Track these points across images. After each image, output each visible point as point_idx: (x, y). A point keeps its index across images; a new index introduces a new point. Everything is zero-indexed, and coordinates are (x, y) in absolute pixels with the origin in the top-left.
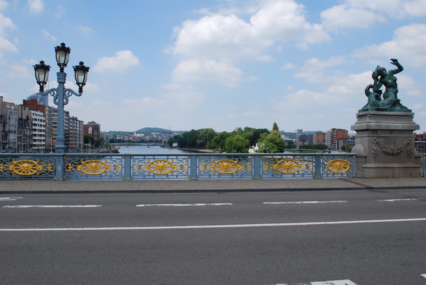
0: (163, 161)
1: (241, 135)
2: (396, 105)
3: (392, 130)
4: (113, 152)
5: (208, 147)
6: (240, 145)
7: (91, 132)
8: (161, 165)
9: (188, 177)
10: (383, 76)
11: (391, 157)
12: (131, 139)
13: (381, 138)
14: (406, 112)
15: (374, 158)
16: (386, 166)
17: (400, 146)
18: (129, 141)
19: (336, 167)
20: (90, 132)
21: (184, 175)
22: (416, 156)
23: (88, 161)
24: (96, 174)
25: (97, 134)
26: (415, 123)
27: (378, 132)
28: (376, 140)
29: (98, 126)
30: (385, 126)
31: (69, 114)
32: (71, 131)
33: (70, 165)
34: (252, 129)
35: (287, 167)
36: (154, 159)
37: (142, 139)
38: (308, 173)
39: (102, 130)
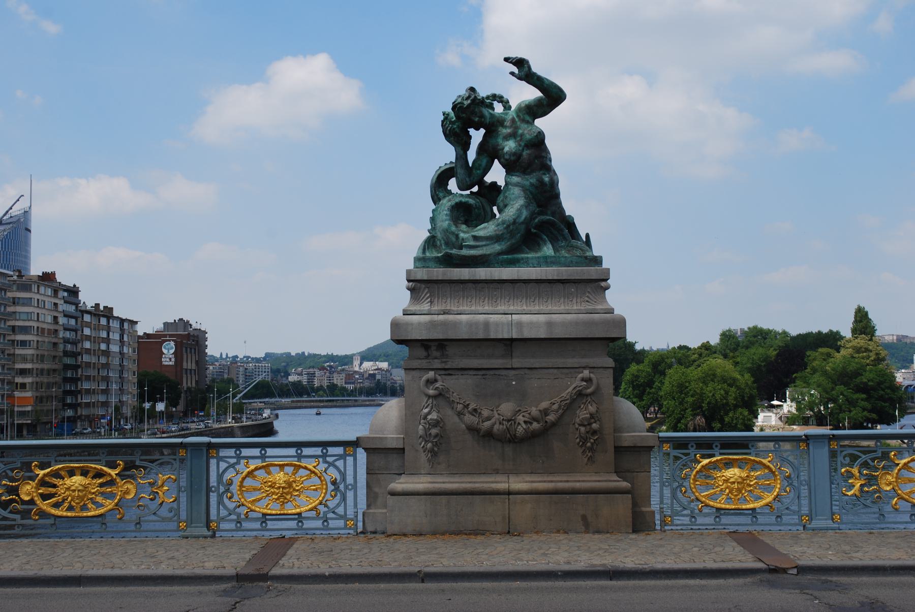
0: (291, 465)
1: (734, 357)
3: (508, 343)
4: (247, 431)
6: (718, 397)
7: (173, 360)
8: (76, 485)
9: (346, 525)
10: (492, 127)
11: (509, 450)
12: (339, 380)
13: (460, 373)
14: (578, 264)
16: (477, 485)
17: (544, 405)
18: (333, 389)
19: (273, 493)
20: (168, 360)
21: (164, 520)
22: (626, 444)
23: (57, 467)
24: (744, 507)
25: (194, 365)
26: (611, 311)
27: (451, 350)
28: (436, 381)
29: (198, 336)
30: (470, 324)
31: (77, 297)
32: (86, 358)
33: (855, 471)
34: (776, 333)
35: (734, 483)
36: (263, 457)
37: (379, 380)
38: (159, 517)
39: (214, 348)
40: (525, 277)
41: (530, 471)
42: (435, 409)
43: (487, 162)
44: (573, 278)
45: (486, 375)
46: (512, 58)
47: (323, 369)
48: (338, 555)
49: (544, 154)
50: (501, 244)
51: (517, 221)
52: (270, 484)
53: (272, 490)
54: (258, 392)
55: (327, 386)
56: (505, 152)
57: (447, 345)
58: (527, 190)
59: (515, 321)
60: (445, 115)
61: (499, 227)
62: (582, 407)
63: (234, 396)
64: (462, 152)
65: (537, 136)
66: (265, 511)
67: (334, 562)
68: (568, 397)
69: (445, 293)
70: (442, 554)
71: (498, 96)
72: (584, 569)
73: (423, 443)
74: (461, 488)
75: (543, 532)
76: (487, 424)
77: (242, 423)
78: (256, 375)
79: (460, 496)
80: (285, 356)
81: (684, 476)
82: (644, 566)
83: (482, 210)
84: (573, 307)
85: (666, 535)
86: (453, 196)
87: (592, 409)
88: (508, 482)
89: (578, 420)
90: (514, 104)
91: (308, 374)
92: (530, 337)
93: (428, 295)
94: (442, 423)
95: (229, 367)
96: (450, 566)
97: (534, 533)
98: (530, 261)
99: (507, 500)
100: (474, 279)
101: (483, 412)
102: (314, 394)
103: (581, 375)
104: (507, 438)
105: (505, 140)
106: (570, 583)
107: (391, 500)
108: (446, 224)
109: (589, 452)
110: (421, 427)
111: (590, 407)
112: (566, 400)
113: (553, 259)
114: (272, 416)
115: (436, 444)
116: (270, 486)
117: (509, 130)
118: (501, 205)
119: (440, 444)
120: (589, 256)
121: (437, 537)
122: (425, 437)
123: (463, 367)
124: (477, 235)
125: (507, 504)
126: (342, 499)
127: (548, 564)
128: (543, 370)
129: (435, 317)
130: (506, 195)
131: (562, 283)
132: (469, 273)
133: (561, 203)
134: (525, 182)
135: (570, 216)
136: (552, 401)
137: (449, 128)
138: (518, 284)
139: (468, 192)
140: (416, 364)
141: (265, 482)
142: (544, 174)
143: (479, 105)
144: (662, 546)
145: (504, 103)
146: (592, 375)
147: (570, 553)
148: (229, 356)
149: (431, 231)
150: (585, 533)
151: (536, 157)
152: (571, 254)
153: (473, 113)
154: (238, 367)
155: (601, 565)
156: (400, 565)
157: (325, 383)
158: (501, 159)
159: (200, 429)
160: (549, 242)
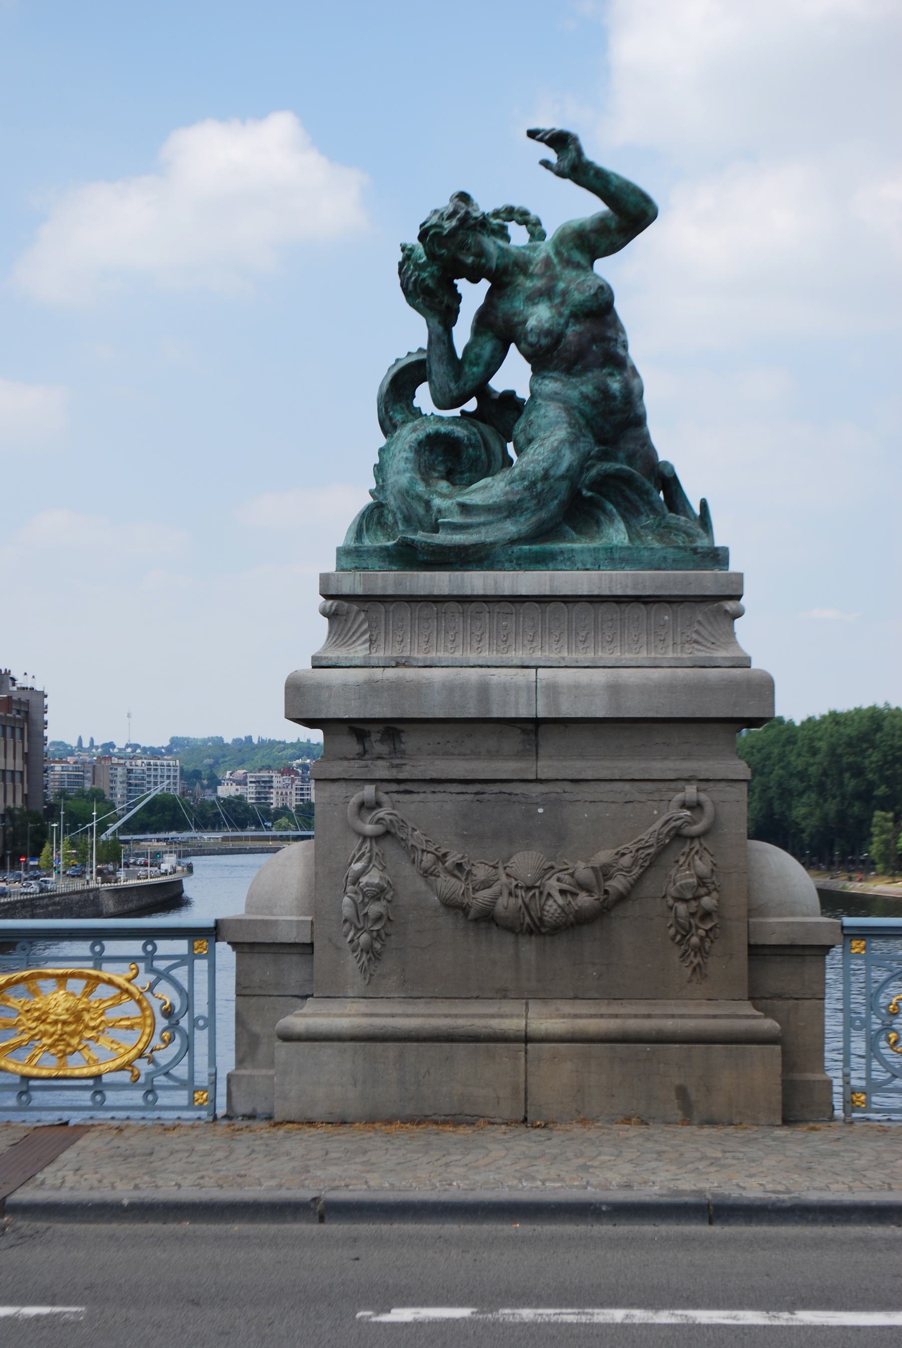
0: (80, 976)
2: (604, 511)
3: (530, 727)
5: (884, 857)
9: (192, 1100)
11: (529, 948)
14: (677, 565)
15: (364, 958)
16: (461, 1022)
17: (604, 856)
22: (773, 940)
26: (744, 663)
27: (410, 741)
28: (378, 804)
29: (27, 704)
30: (450, 688)
40: (567, 590)
41: (571, 994)
42: (376, 864)
43: (495, 349)
44: (667, 593)
45: (482, 793)
46: (543, 130)
47: (288, 771)
48: (160, 1163)
49: (610, 333)
50: (517, 522)
51: (552, 473)
52: (36, 1014)
53: (42, 1027)
54: (153, 818)
55: (297, 807)
56: (529, 329)
57: (403, 732)
58: (573, 408)
59: (544, 683)
60: (406, 252)
61: (514, 485)
62: (681, 863)
63: (102, 828)
64: (440, 329)
65: (595, 295)
66: (27, 1070)
67: (146, 1178)
68: (652, 841)
69: (400, 624)
70: (373, 1164)
71: (518, 211)
72: (655, 1199)
73: (351, 933)
74: (427, 1026)
75: (595, 1120)
76: (484, 895)
77: (116, 882)
78: (149, 782)
79: (424, 1044)
80: (210, 744)
81: (894, 1009)
82: (782, 1196)
83: (483, 449)
84: (665, 653)
85: (851, 1132)
86: (423, 421)
87: (702, 866)
88: (526, 1018)
89: (672, 890)
90: (551, 228)
91: (258, 782)
92: (573, 716)
93: (365, 626)
94: (392, 893)
95: (94, 766)
96: (382, 1189)
97: (577, 1122)
98: (578, 558)
99: (523, 1053)
100: (461, 593)
101: (475, 871)
102: (269, 824)
103: (679, 796)
104: (525, 926)
105: (530, 303)
106: (624, 1229)
107: (283, 1050)
108: (404, 480)
109: (695, 956)
110: (346, 900)
111: (698, 862)
112: (649, 847)
113: (625, 553)
114: (179, 868)
115: (379, 935)
116: (37, 1019)
117: (539, 283)
118: (521, 439)
119: (387, 935)
120: (702, 548)
121: (374, 1128)
122: (356, 921)
123: (435, 775)
124: (468, 502)
125: (523, 1061)
126: (185, 1047)
127: (585, 1188)
128: (602, 784)
129: (378, 673)
130: (532, 418)
131: (646, 603)
132: (450, 581)
133: (647, 436)
134: (569, 392)
135: (666, 463)
136: (619, 849)
137: (413, 278)
138: (553, 605)
139: (456, 412)
140: (338, 769)
141: (28, 1011)
142: (611, 375)
143: (475, 230)
144: (834, 1154)
145: (529, 226)
146: (703, 797)
147: (637, 1165)
148: (96, 744)
149: (376, 494)
150: (683, 1125)
151: (594, 340)
152: (665, 542)
153: (463, 246)
154: (114, 767)
155: (694, 1191)
156: (280, 1186)
157: (293, 802)
158: (521, 343)
159: (30, 893)
160: (619, 518)
